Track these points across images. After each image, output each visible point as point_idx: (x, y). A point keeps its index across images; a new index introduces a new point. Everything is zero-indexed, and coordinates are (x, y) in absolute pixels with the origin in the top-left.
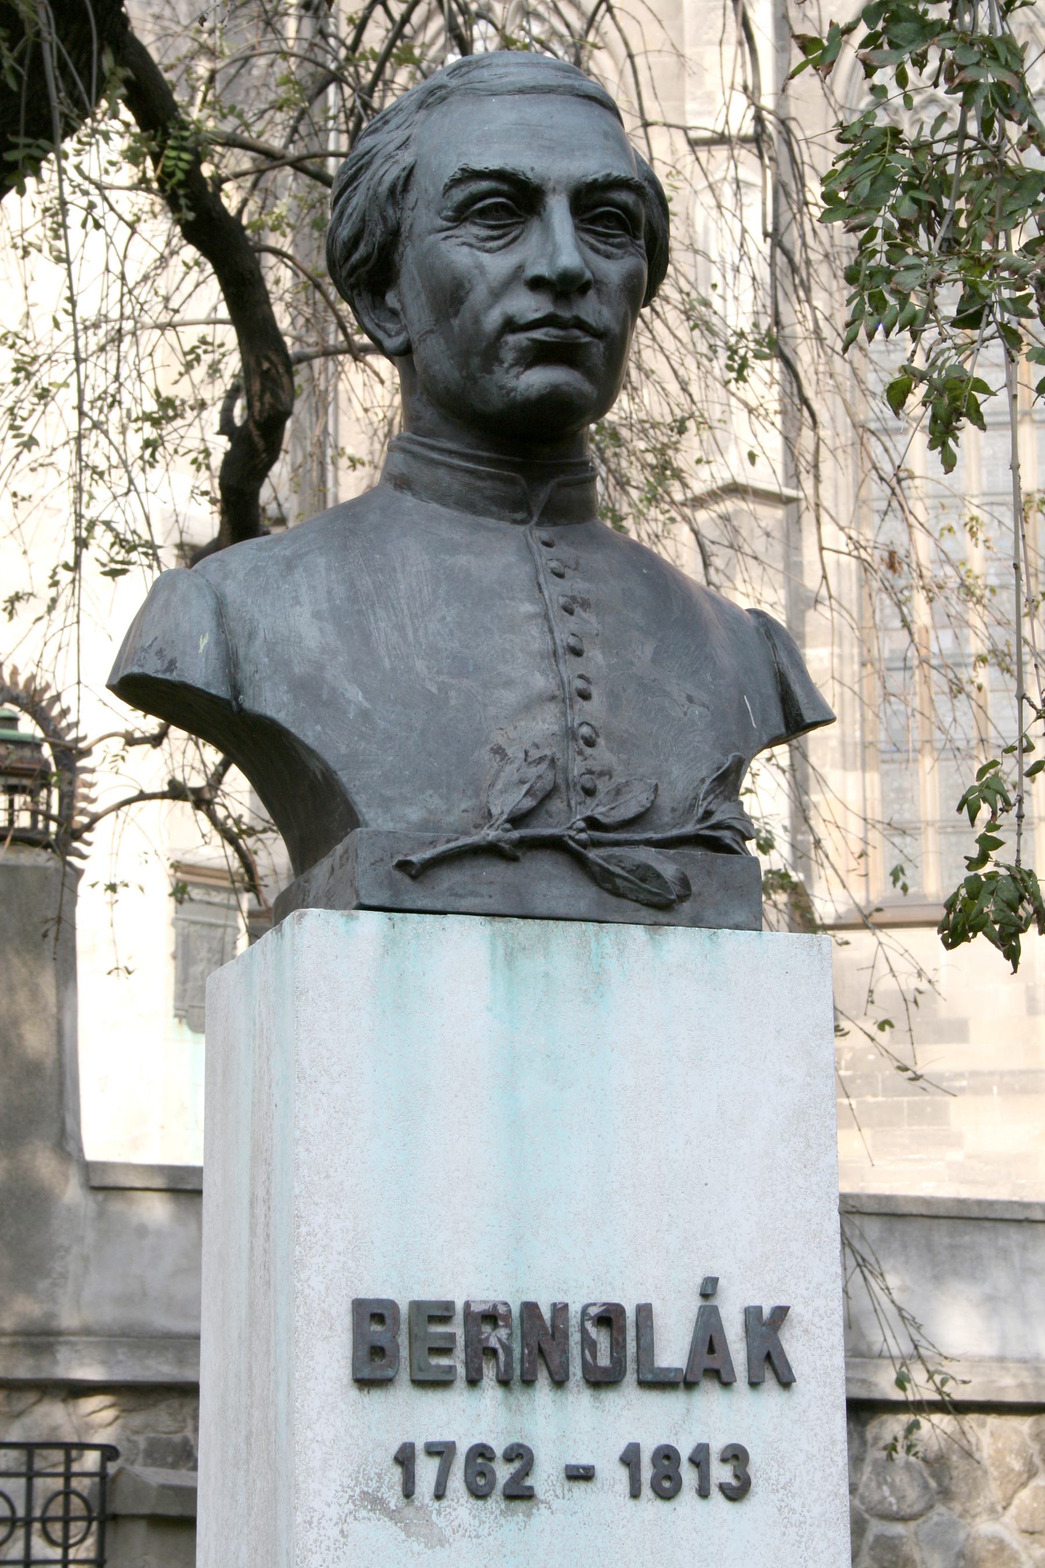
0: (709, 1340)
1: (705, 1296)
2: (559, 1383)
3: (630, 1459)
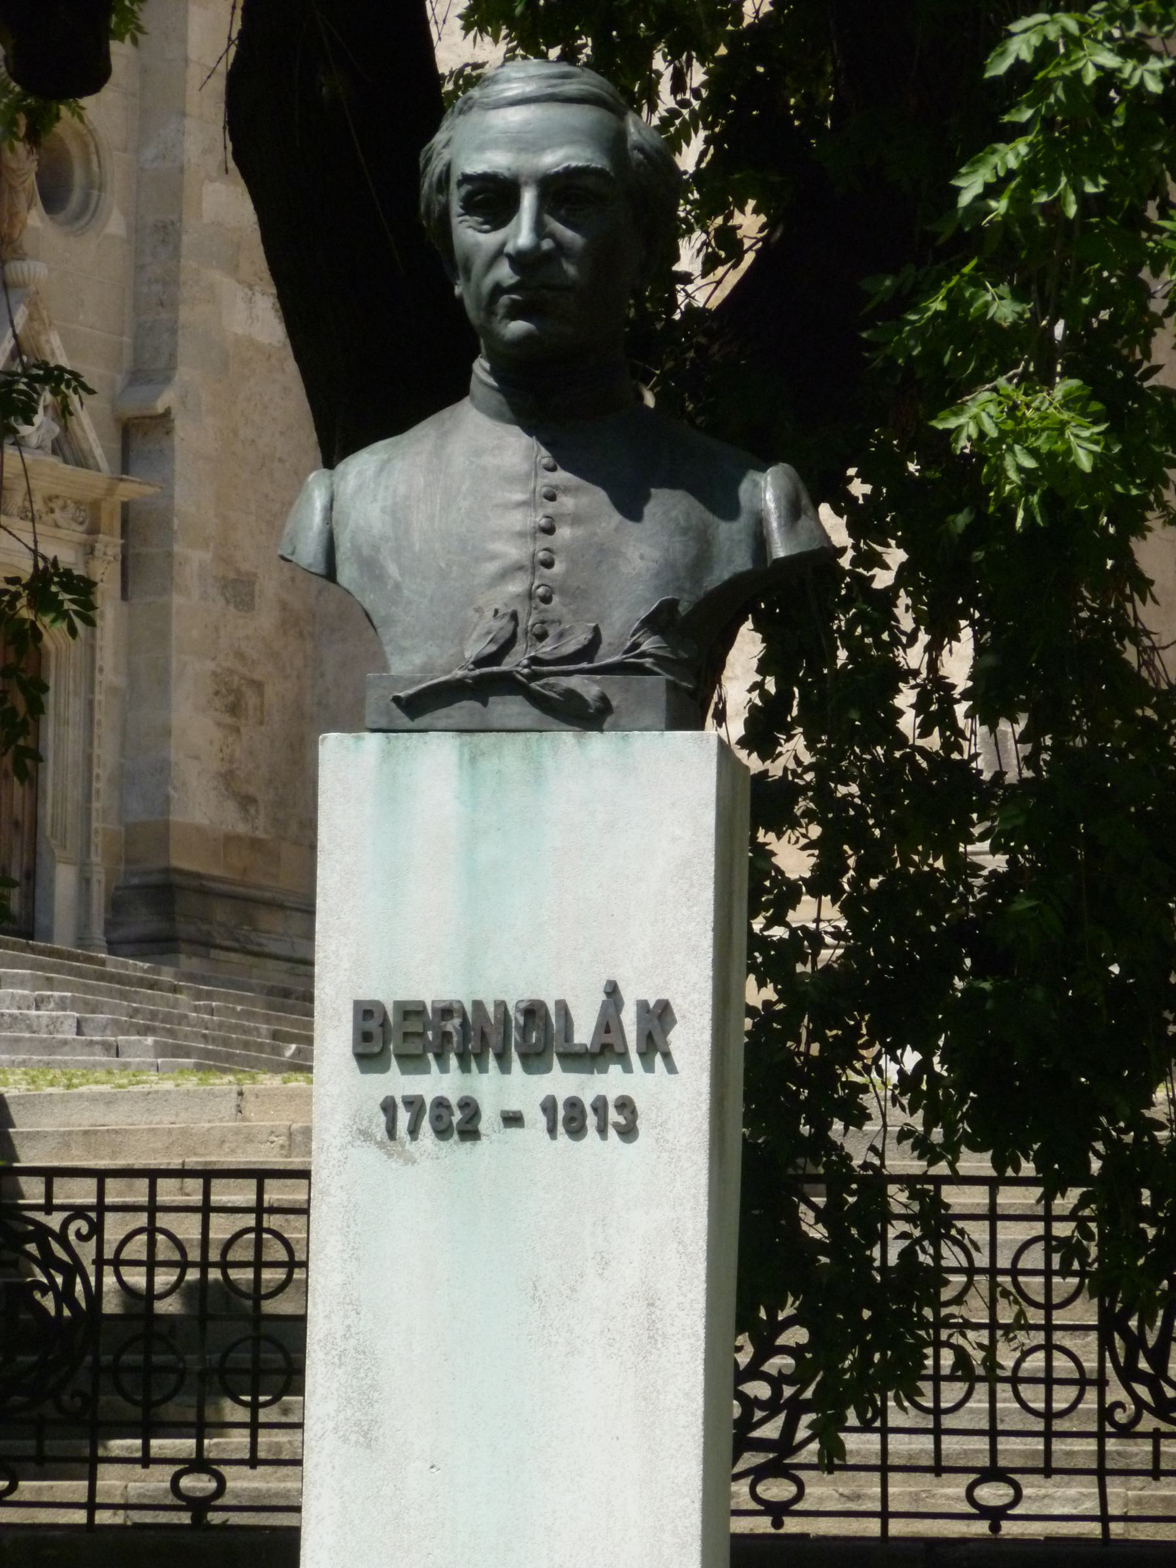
0: (608, 1023)
1: (608, 994)
2: (503, 1059)
3: (549, 1107)
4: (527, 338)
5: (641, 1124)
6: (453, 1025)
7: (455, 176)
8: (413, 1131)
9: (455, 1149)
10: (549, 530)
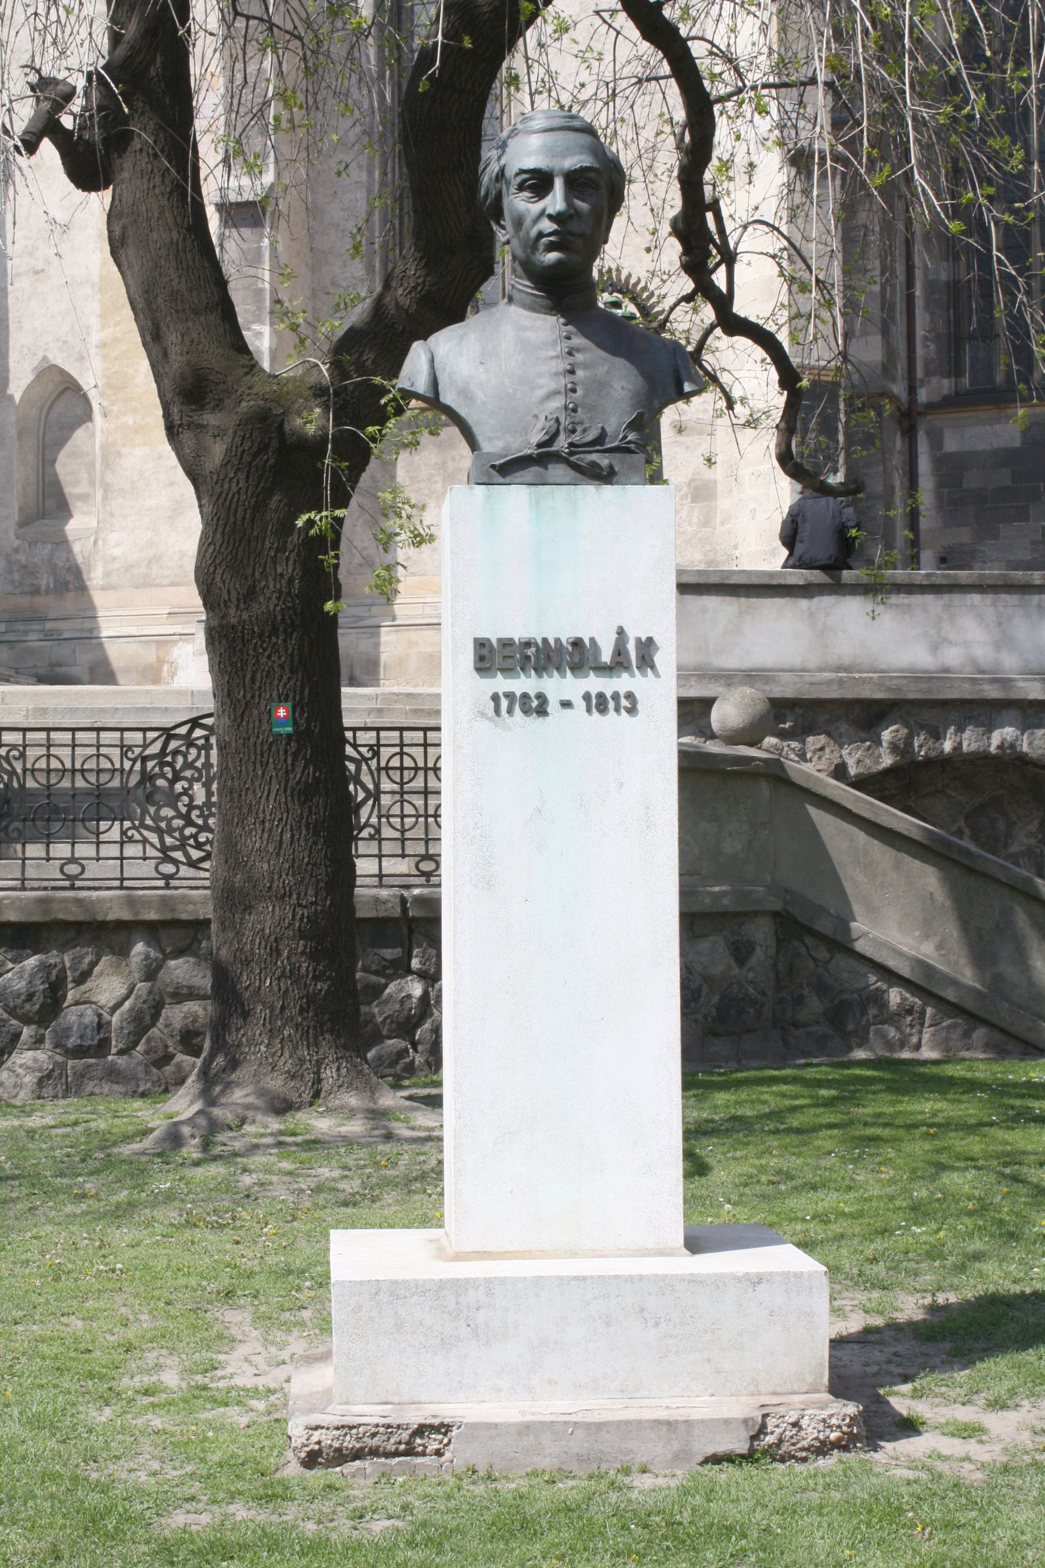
0: (620, 651)
3: (587, 697)
4: (559, 263)
5: (639, 706)
6: (531, 651)
7: (510, 172)
8: (510, 711)
9: (534, 721)
10: (572, 372)
